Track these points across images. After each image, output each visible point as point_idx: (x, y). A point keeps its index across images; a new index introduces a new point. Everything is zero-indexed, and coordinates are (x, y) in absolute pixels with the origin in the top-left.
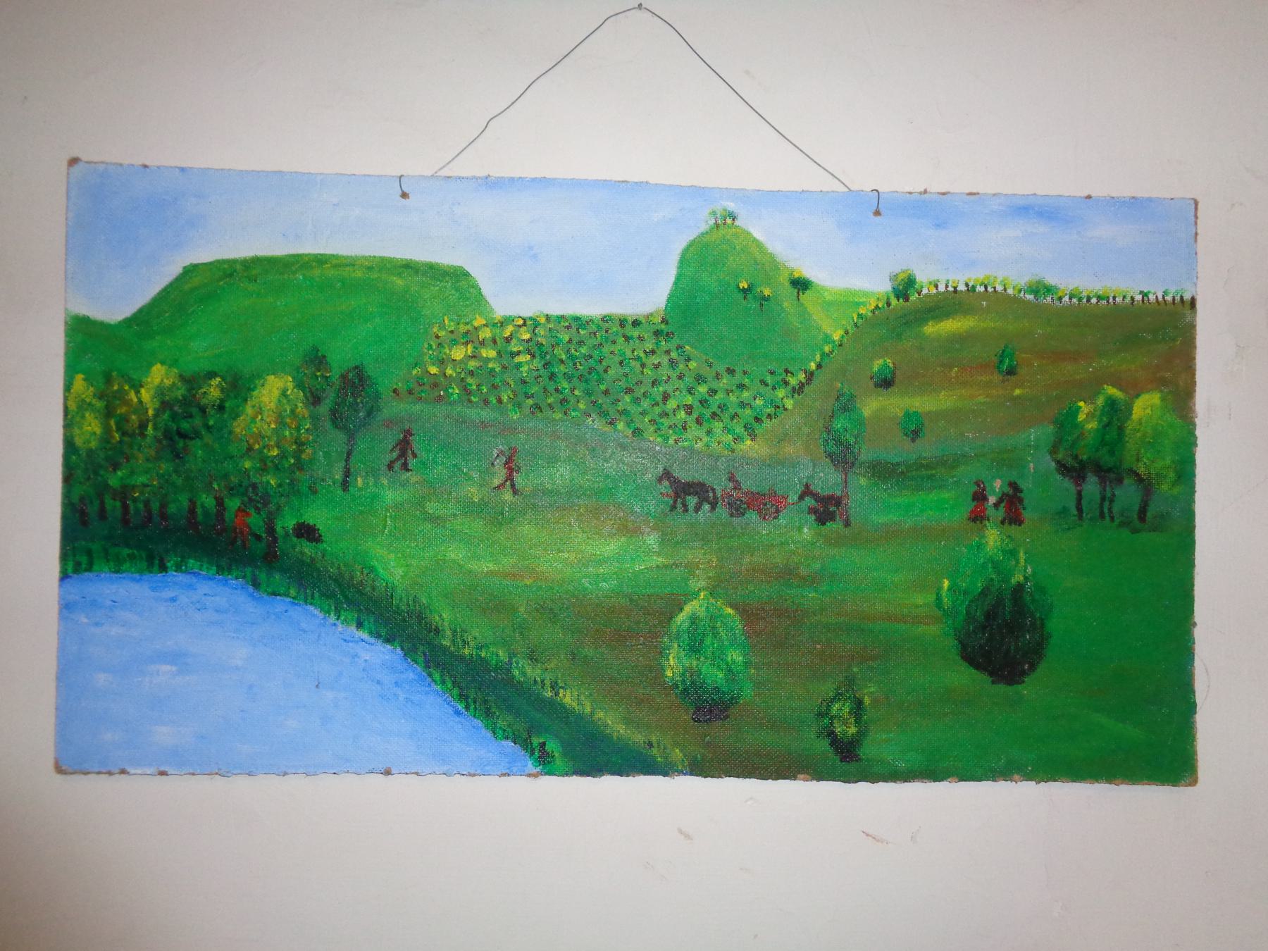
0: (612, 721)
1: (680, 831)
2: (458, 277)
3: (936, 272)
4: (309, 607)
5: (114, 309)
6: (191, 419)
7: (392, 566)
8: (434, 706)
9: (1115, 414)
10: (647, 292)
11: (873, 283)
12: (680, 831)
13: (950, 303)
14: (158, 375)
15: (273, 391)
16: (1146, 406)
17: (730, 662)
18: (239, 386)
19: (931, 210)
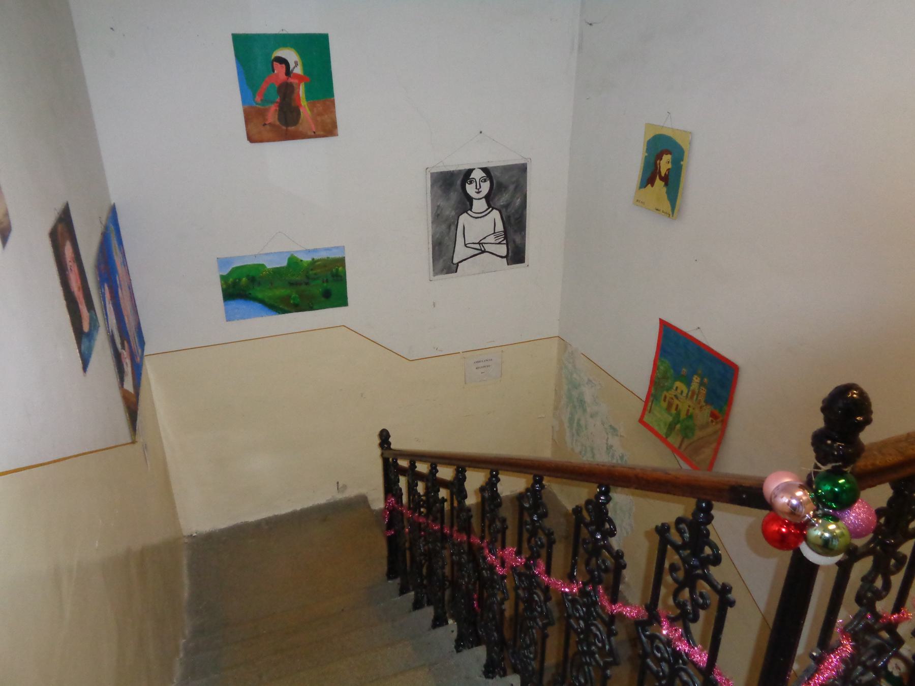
0: (286, 308)
1: (85, 368)
2: (263, 265)
3: (316, 257)
4: (871, 535)
5: (225, 274)
6: (235, 284)
7: (260, 296)
8: (266, 309)
9: (337, 270)
10: (284, 263)
11: (310, 259)
12: (85, 368)
13: (318, 260)
14: (231, 280)
15: (244, 279)
16: (340, 269)
17: (298, 301)
18: (240, 280)
19: (315, 251)
